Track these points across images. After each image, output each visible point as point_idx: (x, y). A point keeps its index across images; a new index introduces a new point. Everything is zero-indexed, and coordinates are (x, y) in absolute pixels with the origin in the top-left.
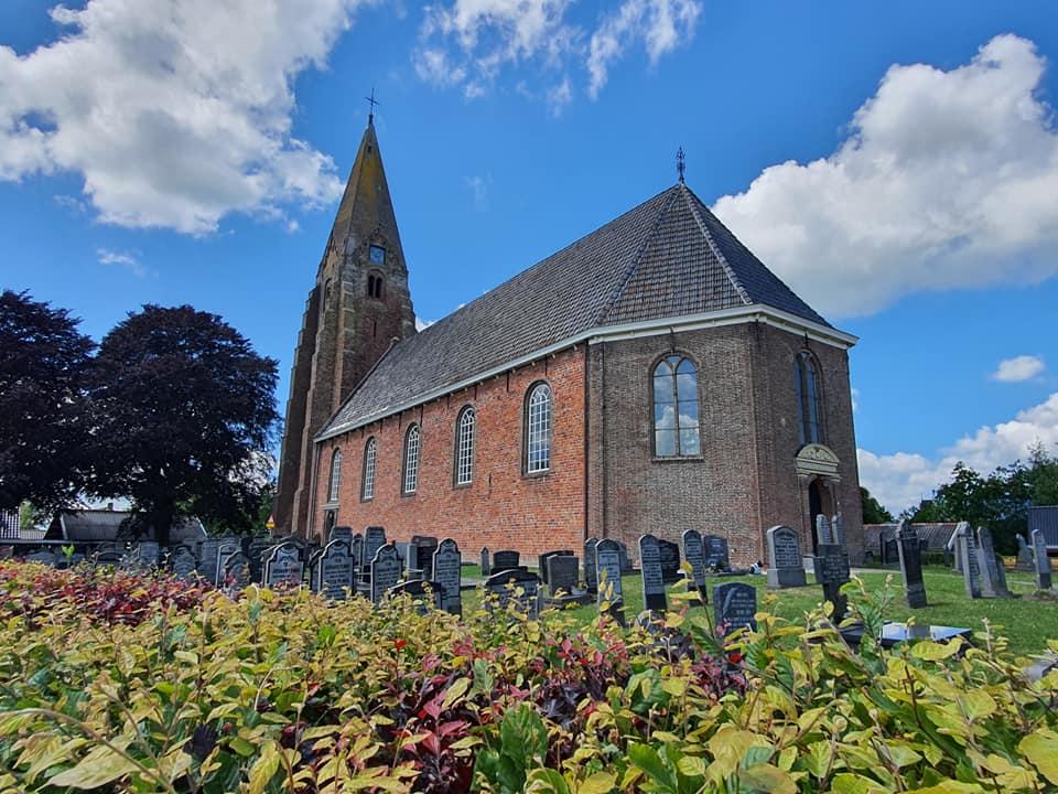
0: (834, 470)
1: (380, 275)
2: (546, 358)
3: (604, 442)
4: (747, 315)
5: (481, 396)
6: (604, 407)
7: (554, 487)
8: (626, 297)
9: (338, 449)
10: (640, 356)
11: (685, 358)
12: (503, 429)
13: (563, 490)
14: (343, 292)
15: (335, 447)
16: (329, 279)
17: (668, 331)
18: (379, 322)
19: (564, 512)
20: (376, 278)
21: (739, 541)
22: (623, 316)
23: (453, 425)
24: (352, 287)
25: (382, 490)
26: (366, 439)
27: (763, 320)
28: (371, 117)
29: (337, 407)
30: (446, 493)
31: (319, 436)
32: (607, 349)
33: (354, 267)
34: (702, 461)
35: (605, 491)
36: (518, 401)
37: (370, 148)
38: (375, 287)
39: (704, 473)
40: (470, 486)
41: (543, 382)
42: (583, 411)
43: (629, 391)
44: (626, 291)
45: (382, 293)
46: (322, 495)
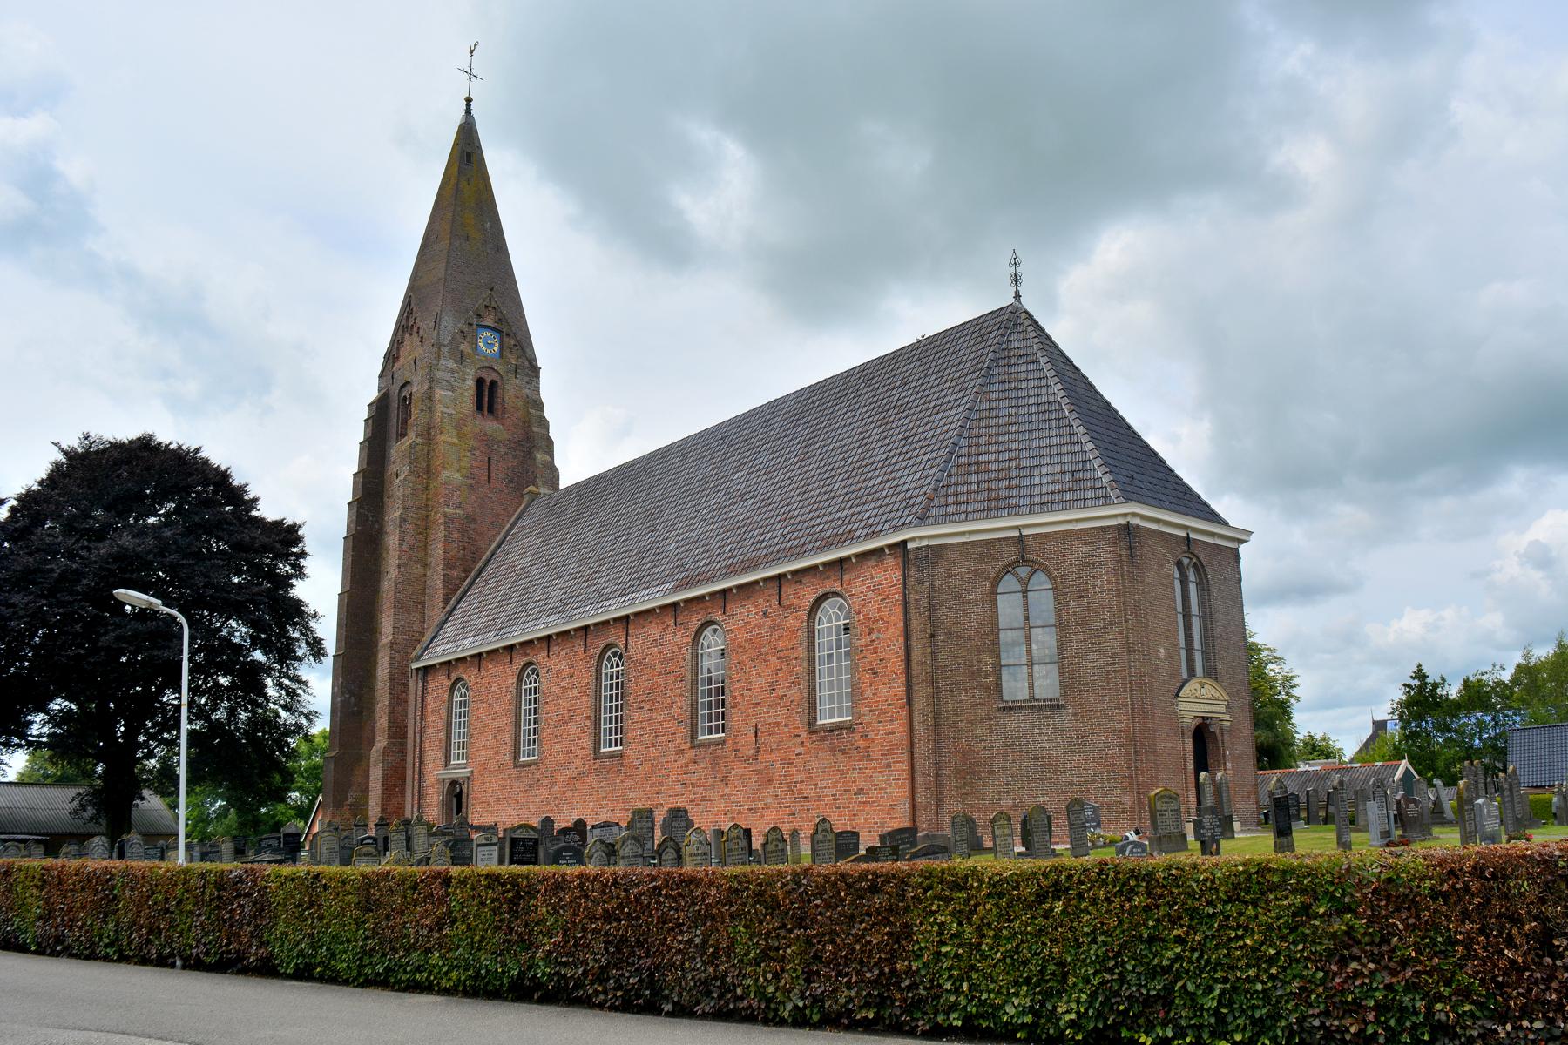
0: (1223, 709)
1: (494, 376)
2: (841, 562)
3: (933, 683)
4: (1115, 516)
5: (733, 608)
6: (932, 636)
7: (861, 743)
8: (954, 480)
10: (978, 566)
11: (1037, 568)
13: (876, 747)
14: (439, 408)
15: (454, 676)
17: (1016, 533)
18: (495, 457)
19: (879, 778)
21: (1110, 807)
22: (952, 509)
23: (687, 651)
24: (453, 398)
25: (557, 748)
27: (1136, 521)
28: (469, 100)
29: (437, 614)
31: (418, 658)
32: (933, 554)
33: (452, 364)
35: (937, 748)
36: (797, 620)
37: (469, 155)
38: (487, 396)
39: (1066, 721)
40: (723, 742)
41: (836, 594)
42: (901, 640)
43: (965, 613)
44: (954, 471)
45: (498, 406)
46: (433, 755)
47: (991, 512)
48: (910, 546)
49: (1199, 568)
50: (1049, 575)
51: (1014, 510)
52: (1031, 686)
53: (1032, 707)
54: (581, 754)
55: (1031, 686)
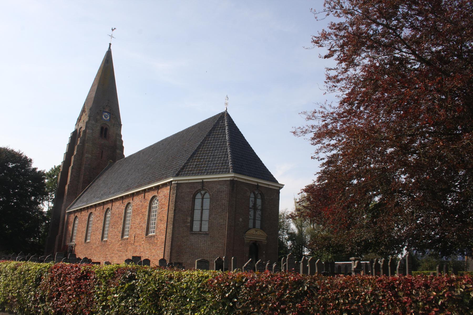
0: (265, 239)
9: (77, 216)
12: (141, 215)
13: (159, 243)
16: (81, 128)
17: (201, 181)
20: (105, 128)
23: (124, 211)
26: (89, 213)
28: (110, 44)
30: (119, 241)
31: (69, 209)
33: (93, 122)
34: (208, 234)
36: (147, 204)
47: (198, 174)
48: (173, 183)
49: (262, 195)
50: (209, 194)
51: (202, 174)
52: (201, 227)
53: (199, 234)
54: (98, 240)
55: (201, 227)
